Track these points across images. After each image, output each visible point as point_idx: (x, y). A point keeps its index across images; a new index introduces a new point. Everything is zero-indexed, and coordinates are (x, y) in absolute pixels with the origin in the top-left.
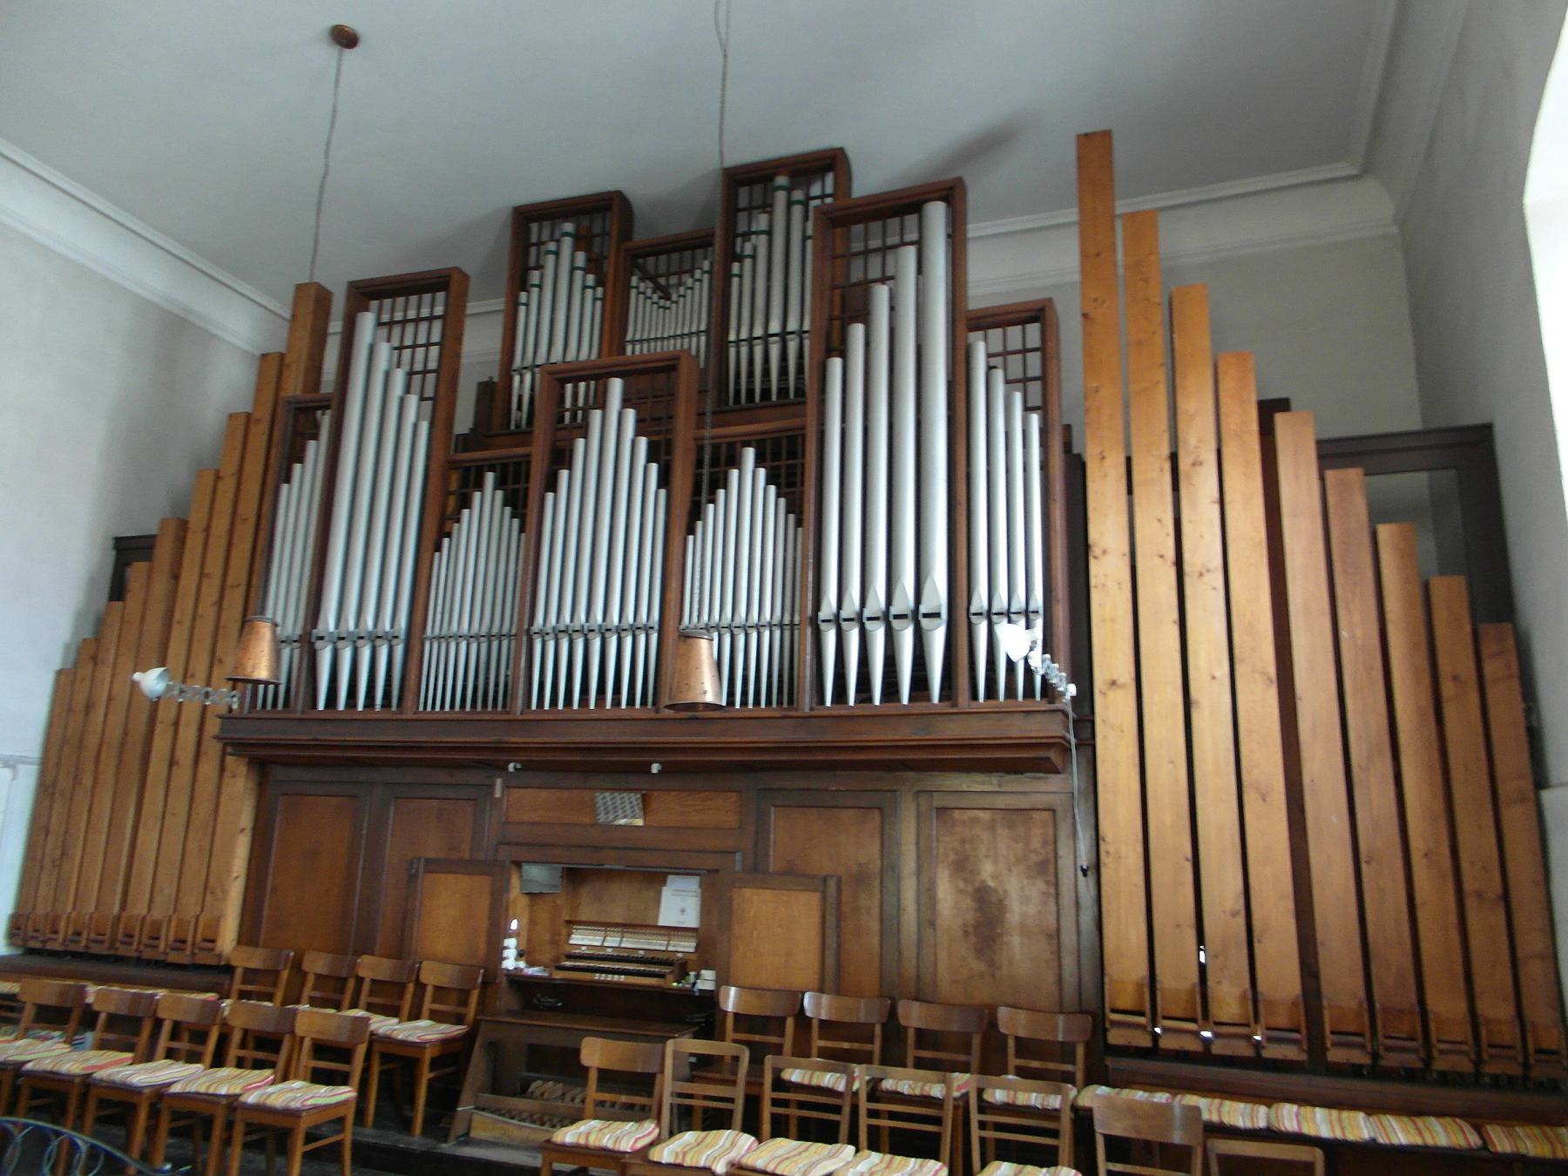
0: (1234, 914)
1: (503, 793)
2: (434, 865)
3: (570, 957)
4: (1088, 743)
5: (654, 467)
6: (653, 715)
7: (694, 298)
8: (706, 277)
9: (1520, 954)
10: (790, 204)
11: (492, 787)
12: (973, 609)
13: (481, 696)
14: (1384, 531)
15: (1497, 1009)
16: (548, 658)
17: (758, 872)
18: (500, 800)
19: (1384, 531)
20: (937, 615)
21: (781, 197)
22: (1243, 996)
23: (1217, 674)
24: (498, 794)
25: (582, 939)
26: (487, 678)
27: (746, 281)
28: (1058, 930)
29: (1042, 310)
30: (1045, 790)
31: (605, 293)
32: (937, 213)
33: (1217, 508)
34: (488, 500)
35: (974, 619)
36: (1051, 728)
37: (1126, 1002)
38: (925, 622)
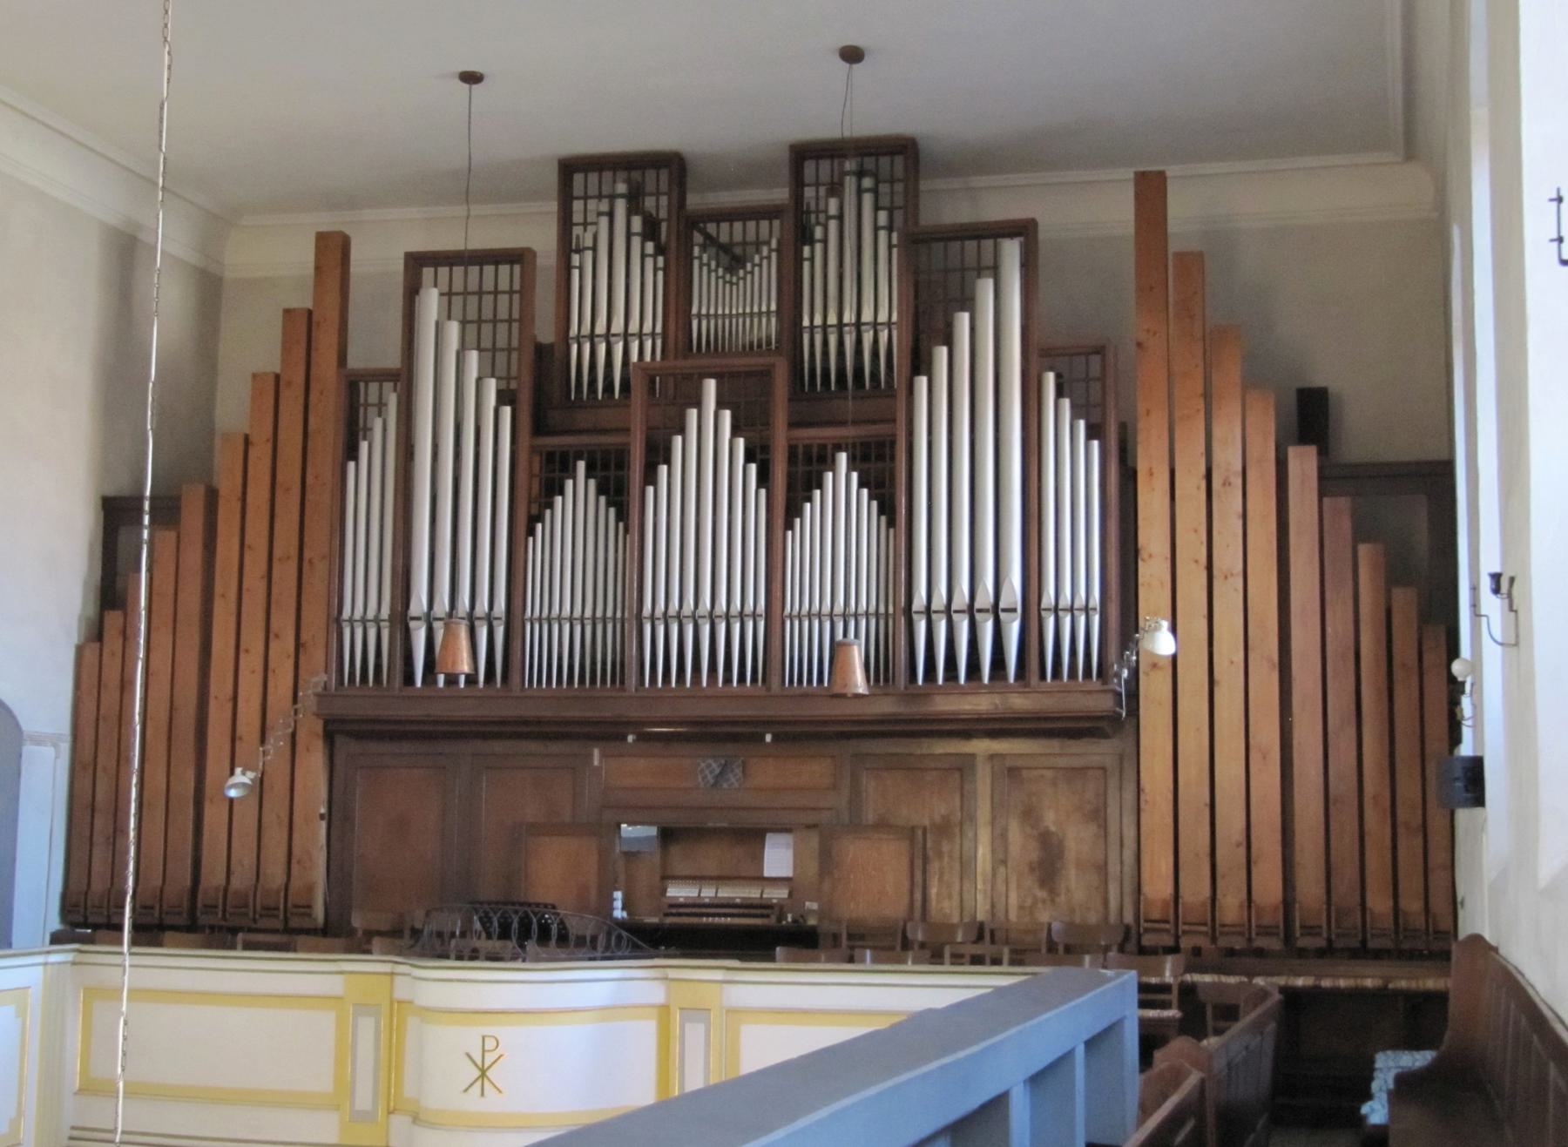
0: (1238, 845)
1: (601, 762)
2: (537, 829)
3: (671, 906)
4: (1134, 711)
5: (753, 467)
6: (764, 693)
7: (763, 276)
8: (774, 255)
9: (1430, 865)
10: (860, 192)
11: (591, 755)
12: (1043, 606)
13: (590, 674)
14: (1363, 549)
15: (1412, 905)
16: (655, 638)
17: (856, 827)
18: (599, 769)
19: (1363, 549)
20: (1014, 610)
21: (850, 183)
22: (1241, 906)
23: (1235, 659)
24: (596, 763)
25: (678, 892)
26: (594, 663)
27: (818, 264)
28: (1106, 864)
29: (1103, 347)
30: (1097, 752)
31: (666, 262)
32: (1011, 251)
33: (1240, 523)
34: (579, 490)
35: (1043, 613)
36: (1104, 704)
37: (1156, 915)
38: (1003, 616)
